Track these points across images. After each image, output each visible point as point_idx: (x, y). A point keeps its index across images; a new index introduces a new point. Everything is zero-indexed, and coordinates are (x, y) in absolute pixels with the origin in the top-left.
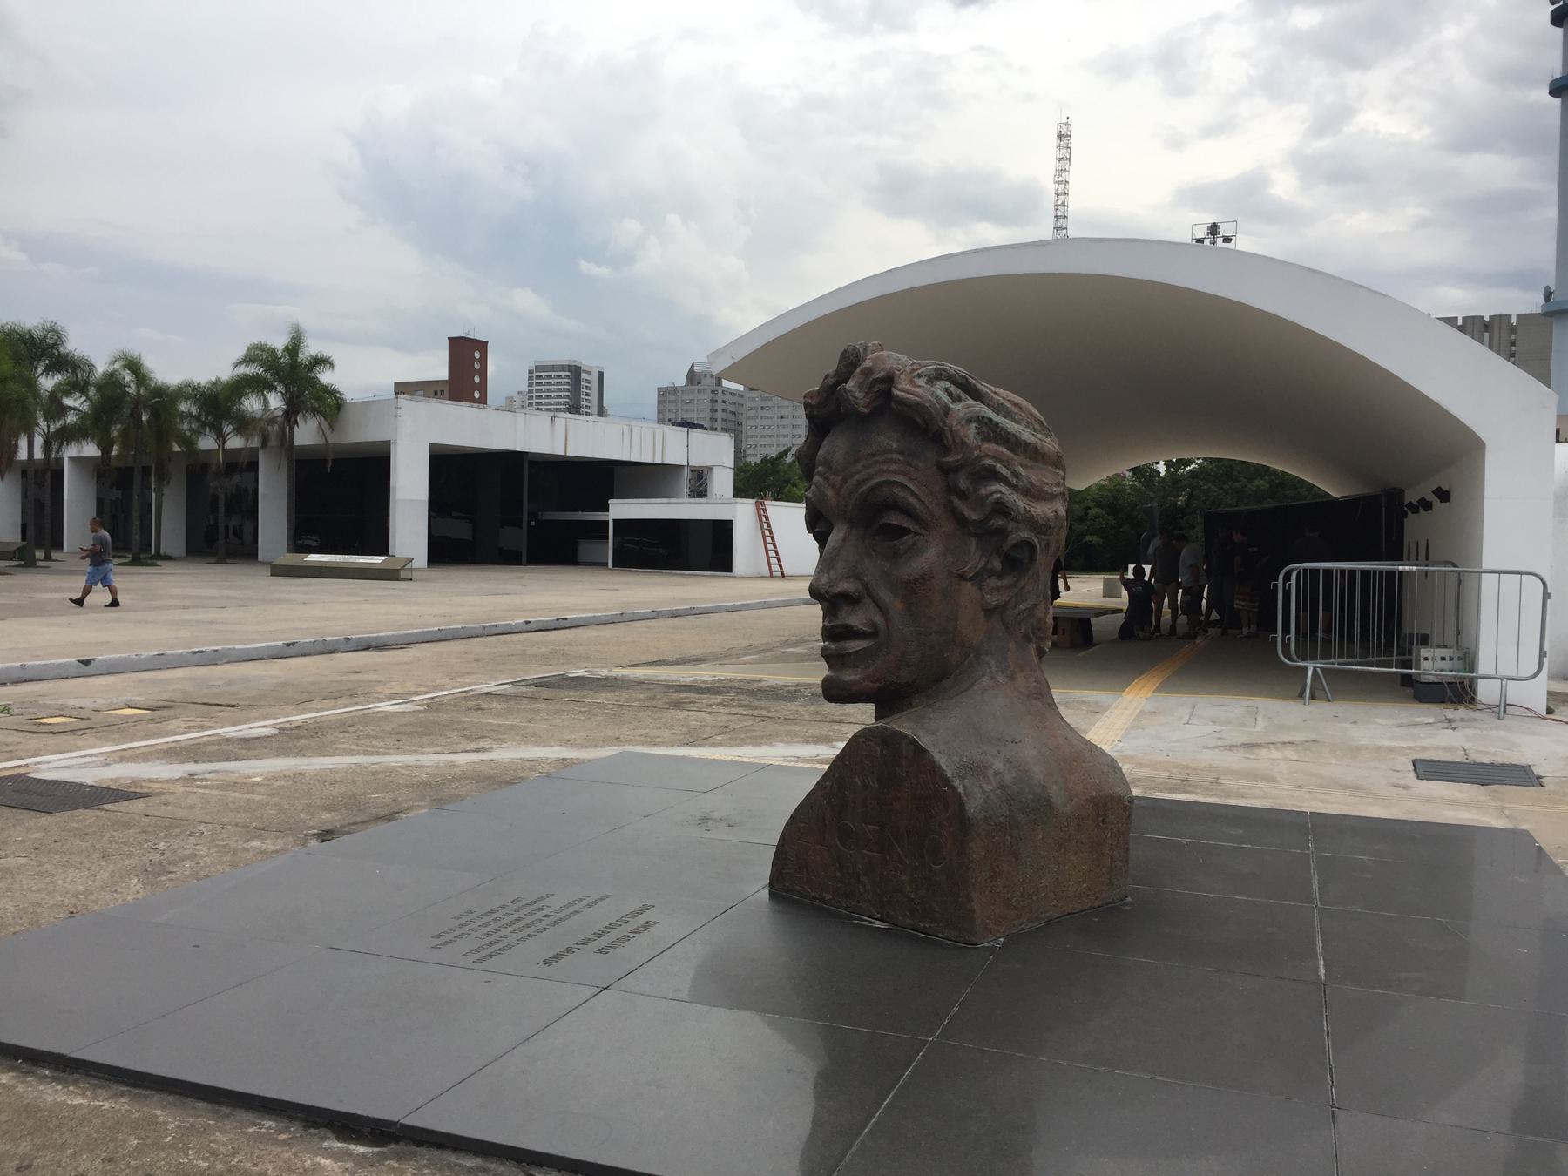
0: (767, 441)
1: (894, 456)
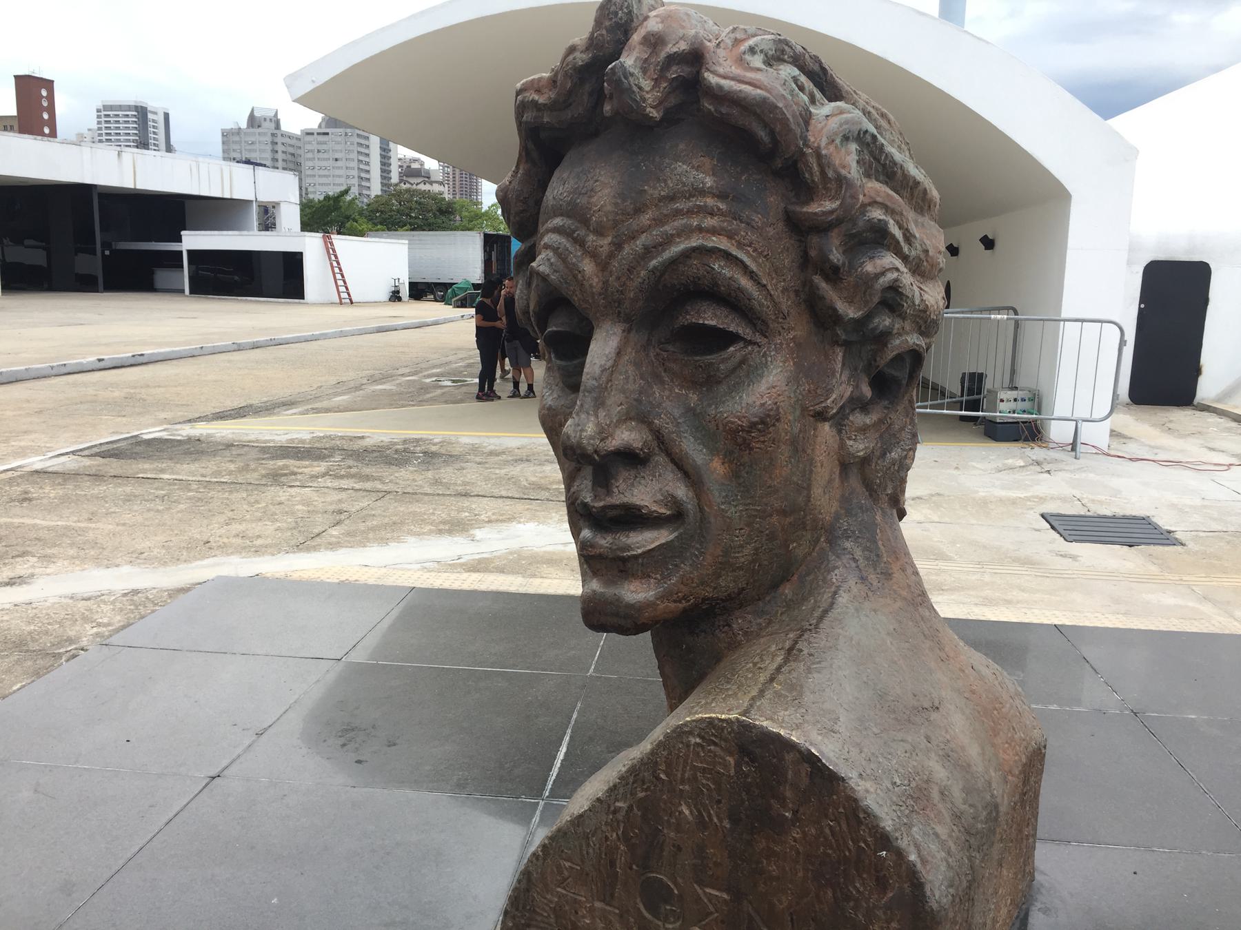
1: (710, 201)
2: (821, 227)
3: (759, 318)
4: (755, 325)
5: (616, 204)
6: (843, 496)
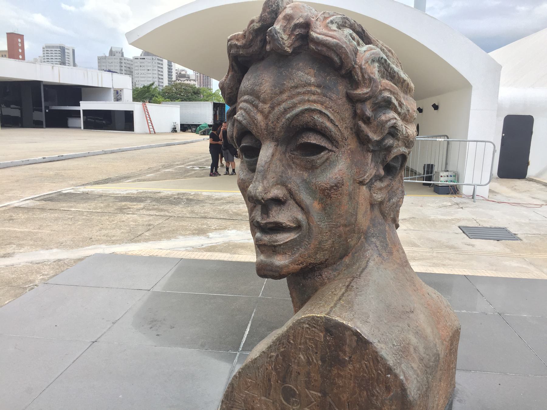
0: (143, 79)
1: (313, 89)
2: (362, 100)
3: (334, 140)
5: (272, 90)
6: (371, 218)
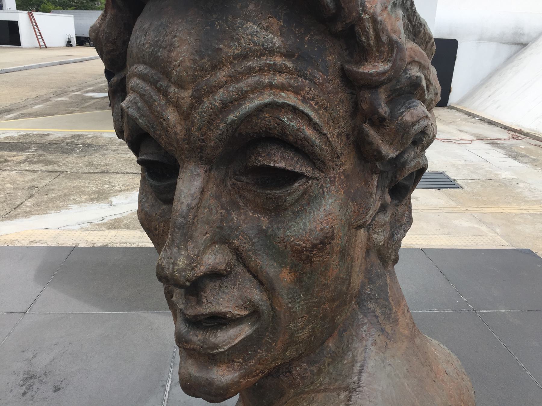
1: (279, 60)
2: (372, 84)
3: (319, 160)
4: (314, 164)
5: (194, 61)
6: (366, 269)
